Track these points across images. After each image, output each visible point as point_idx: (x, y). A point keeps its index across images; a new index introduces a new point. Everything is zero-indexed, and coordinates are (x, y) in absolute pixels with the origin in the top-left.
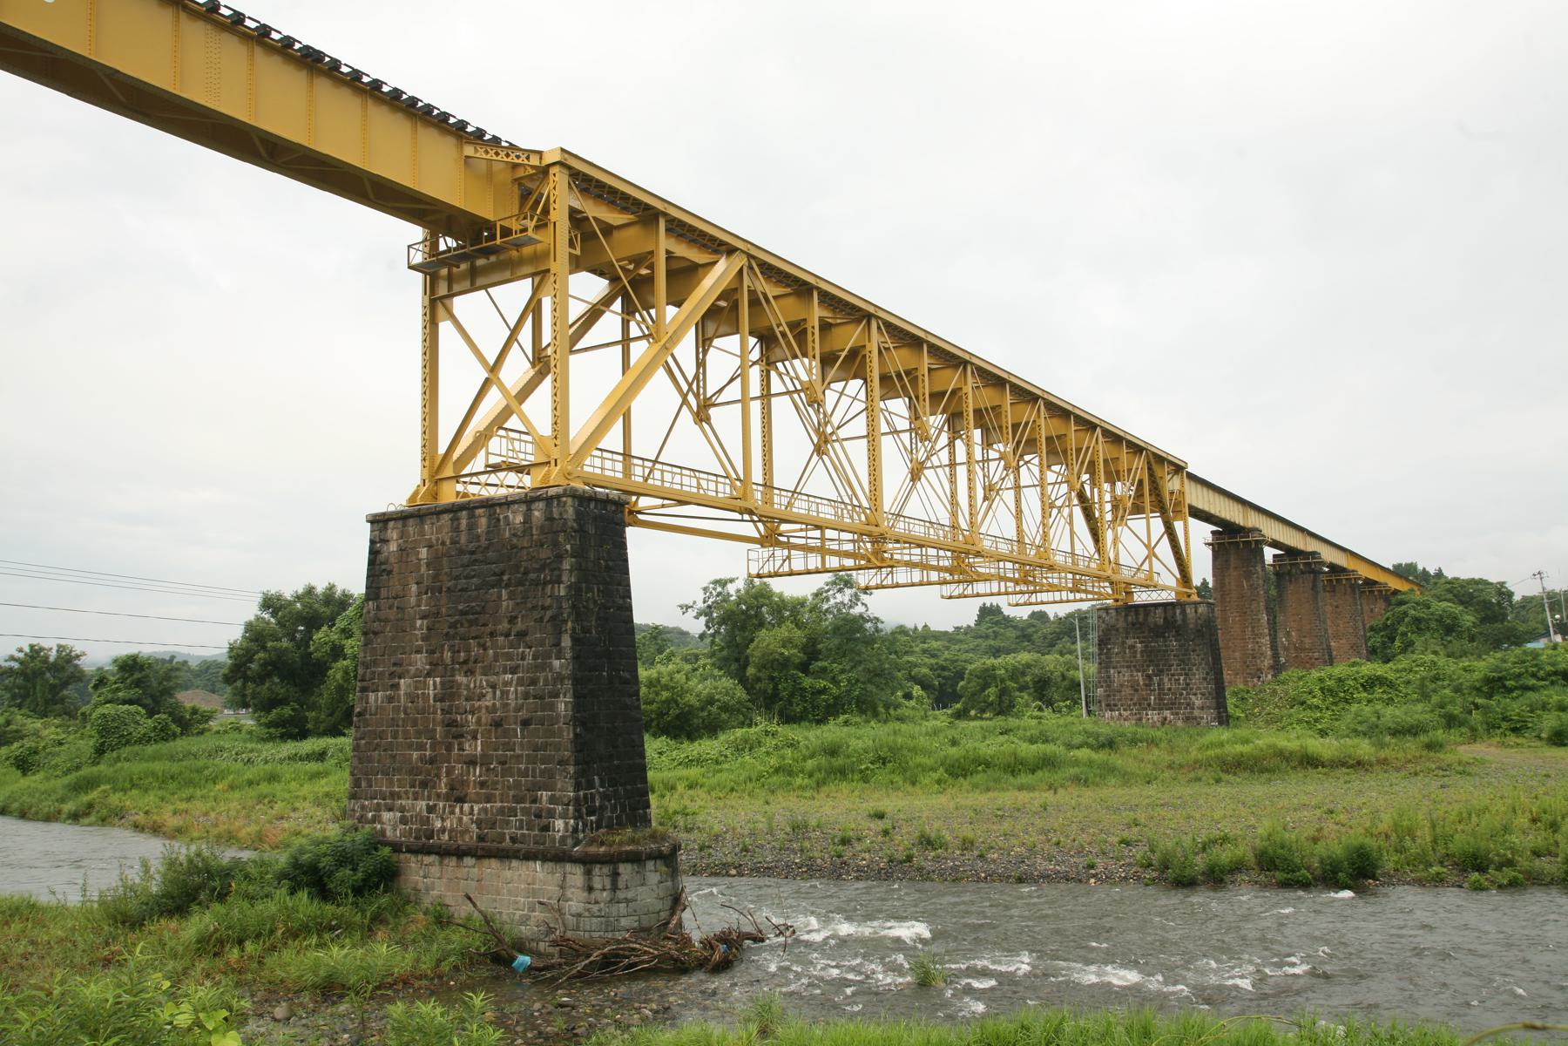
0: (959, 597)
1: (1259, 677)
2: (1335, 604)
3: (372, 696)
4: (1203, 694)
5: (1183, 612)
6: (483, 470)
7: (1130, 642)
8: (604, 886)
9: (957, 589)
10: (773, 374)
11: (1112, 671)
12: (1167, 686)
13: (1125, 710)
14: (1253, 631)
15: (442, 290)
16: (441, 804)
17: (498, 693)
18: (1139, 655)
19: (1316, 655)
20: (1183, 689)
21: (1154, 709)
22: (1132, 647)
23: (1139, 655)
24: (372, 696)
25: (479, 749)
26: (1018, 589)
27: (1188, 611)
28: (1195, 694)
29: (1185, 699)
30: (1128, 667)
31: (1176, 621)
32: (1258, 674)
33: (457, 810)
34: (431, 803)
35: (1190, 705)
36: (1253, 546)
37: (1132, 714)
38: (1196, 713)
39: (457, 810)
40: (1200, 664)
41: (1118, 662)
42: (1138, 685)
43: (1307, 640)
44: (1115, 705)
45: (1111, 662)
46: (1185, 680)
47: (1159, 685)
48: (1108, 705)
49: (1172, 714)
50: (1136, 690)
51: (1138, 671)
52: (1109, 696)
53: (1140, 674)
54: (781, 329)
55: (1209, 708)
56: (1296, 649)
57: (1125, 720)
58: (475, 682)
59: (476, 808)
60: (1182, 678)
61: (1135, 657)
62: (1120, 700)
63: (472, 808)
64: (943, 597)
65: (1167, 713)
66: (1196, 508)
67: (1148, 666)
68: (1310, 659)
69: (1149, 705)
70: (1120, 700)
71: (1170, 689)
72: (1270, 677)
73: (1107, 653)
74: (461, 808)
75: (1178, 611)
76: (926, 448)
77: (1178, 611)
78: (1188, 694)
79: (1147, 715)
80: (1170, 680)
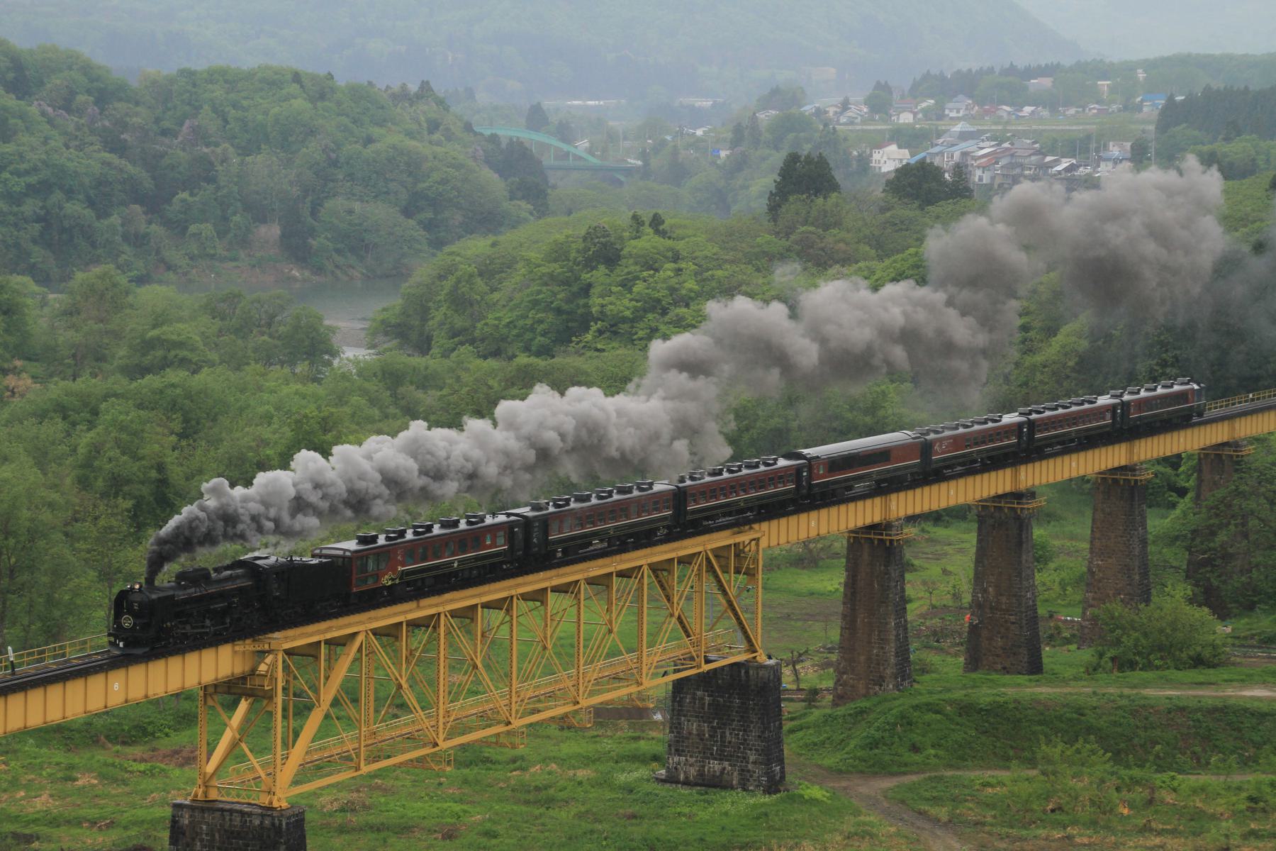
1: (881, 685)
2: (1108, 510)
4: (756, 750)
5: (747, 672)
7: (699, 693)
8: (231, 815)
12: (728, 737)
13: (691, 756)
14: (879, 635)
19: (1012, 618)
21: (716, 759)
22: (702, 699)
27: (751, 672)
28: (751, 750)
29: (742, 753)
30: (697, 717)
31: (740, 680)
32: (880, 681)
35: (745, 759)
36: (888, 544)
37: (696, 761)
38: (750, 767)
40: (757, 723)
41: (688, 711)
43: (1004, 599)
44: (683, 751)
45: (681, 710)
48: (677, 750)
49: (730, 765)
50: (702, 740)
51: (704, 722)
52: (678, 741)
54: (233, 793)
55: (761, 763)
56: (992, 608)
57: (690, 766)
61: (703, 709)
62: (687, 747)
67: (714, 719)
68: (1006, 622)
69: (712, 754)
70: (687, 747)
71: (730, 742)
72: (891, 686)
73: (679, 702)
75: (743, 672)
77: (743, 672)
78: (744, 749)
80: (731, 734)
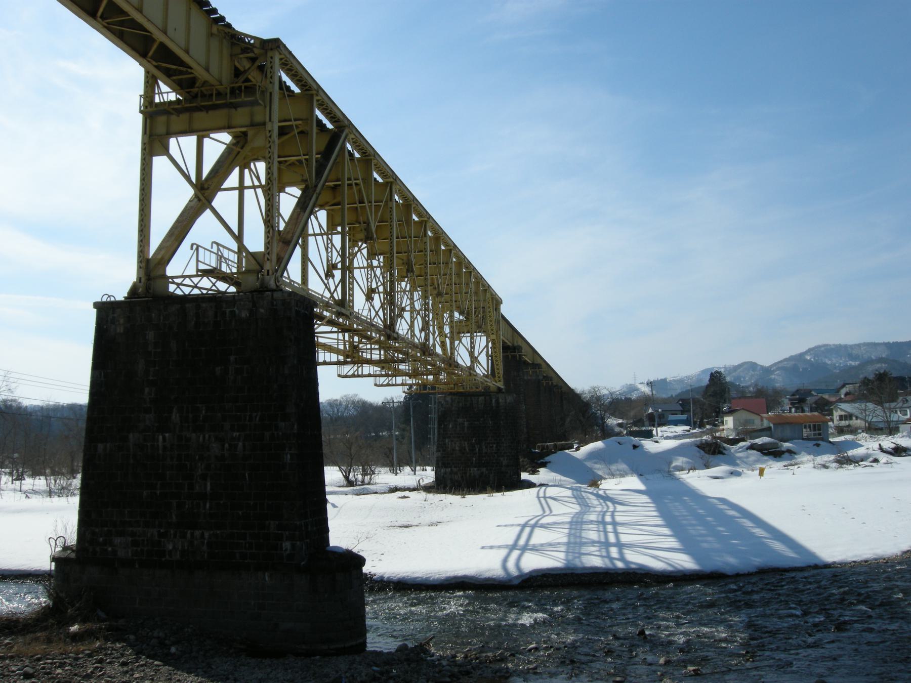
0: (353, 376)
3: (100, 446)
6: (195, 273)
7: (460, 420)
9: (347, 369)
10: (246, 171)
11: (447, 441)
13: (455, 467)
15: (161, 129)
16: (172, 532)
17: (227, 445)
18: (466, 430)
20: (495, 453)
23: (466, 430)
24: (100, 446)
25: (209, 488)
26: (383, 373)
33: (189, 536)
34: (162, 531)
39: (189, 536)
42: (465, 449)
46: (496, 447)
47: (479, 450)
53: (466, 443)
58: (204, 437)
59: (206, 535)
60: (495, 446)
63: (203, 534)
64: (339, 376)
65: (484, 470)
66: (539, 365)
71: (486, 453)
74: (192, 534)
76: (407, 296)
79: (470, 470)
80: (486, 447)
